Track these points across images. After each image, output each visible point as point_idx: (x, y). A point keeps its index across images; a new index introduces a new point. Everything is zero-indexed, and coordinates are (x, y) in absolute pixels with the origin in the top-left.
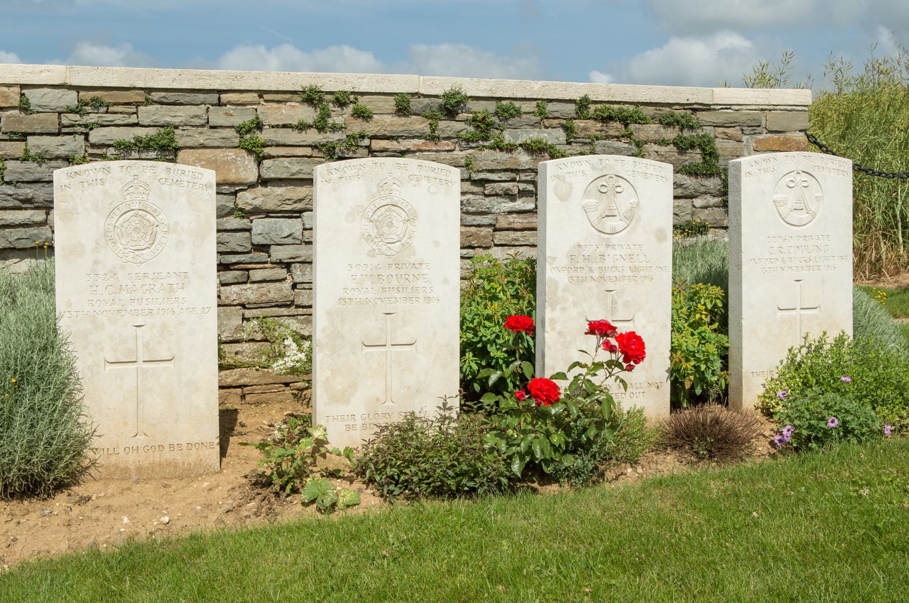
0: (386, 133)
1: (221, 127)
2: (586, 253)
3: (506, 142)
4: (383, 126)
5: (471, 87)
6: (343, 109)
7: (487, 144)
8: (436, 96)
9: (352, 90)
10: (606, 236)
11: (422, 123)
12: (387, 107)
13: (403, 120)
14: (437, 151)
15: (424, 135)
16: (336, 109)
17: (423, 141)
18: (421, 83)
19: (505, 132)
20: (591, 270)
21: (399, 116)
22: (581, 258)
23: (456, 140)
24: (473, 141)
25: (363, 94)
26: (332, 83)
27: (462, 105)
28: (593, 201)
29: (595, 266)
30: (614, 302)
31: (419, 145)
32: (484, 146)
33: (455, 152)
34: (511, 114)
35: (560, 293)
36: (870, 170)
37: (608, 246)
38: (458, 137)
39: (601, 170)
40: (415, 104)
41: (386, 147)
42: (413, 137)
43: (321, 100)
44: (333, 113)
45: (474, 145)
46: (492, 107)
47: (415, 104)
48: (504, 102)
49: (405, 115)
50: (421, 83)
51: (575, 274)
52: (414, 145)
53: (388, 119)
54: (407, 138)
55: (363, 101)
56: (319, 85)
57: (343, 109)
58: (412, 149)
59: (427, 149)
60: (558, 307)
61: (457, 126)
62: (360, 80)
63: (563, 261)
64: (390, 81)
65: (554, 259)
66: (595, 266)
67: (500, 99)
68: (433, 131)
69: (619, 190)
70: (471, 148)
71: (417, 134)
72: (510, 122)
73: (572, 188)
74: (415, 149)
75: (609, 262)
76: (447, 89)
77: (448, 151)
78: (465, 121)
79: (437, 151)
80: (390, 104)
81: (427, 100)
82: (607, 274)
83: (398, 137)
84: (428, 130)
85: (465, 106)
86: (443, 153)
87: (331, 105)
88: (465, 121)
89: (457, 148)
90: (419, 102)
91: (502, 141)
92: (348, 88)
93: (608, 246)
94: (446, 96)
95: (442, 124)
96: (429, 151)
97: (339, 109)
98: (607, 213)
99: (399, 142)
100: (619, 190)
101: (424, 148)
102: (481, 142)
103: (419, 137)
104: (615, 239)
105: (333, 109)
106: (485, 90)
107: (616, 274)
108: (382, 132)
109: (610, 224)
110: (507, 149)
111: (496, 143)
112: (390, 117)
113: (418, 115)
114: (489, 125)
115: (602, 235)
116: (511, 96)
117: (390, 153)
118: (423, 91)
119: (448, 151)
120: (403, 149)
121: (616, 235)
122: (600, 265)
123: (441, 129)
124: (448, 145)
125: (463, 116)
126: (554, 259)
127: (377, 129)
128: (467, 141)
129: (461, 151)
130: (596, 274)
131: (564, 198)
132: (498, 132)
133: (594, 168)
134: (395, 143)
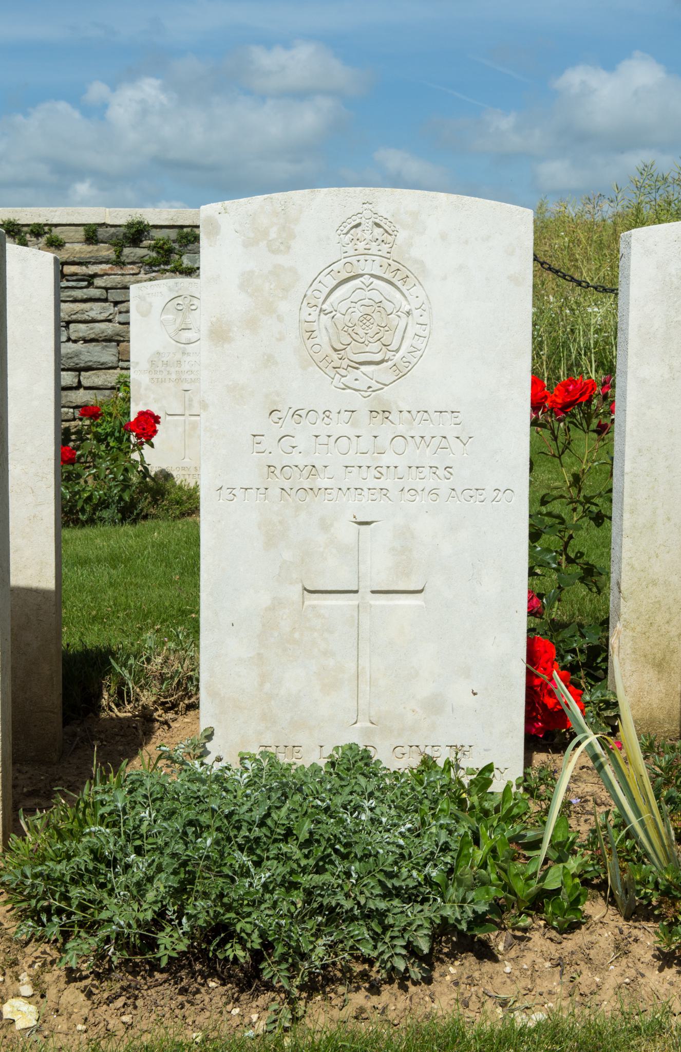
0: (75, 259)
1: (78, 242)
2: (165, 359)
3: (184, 266)
4: (72, 253)
5: (153, 215)
6: (38, 239)
7: (168, 267)
8: (120, 226)
9: (46, 222)
10: (183, 345)
11: (109, 250)
12: (77, 237)
13: (91, 247)
14: (123, 275)
15: (111, 261)
16: (33, 239)
17: (110, 266)
18: (107, 214)
19: (183, 257)
20: (169, 373)
21: (89, 244)
22: (160, 364)
23: (140, 265)
24: (155, 266)
25: (56, 225)
26: (28, 217)
27: (146, 233)
28: (170, 317)
29: (173, 370)
30: (191, 400)
31: (105, 270)
32: (165, 270)
33: (140, 276)
34: (189, 241)
35: (142, 391)
36: (600, 292)
37: (183, 353)
38: (141, 262)
39: (177, 292)
40: (102, 234)
41: (76, 271)
42: (101, 263)
43: (19, 232)
44: (29, 243)
45: (156, 269)
46: (173, 234)
47: (102, 234)
48: (185, 230)
49: (92, 243)
50: (107, 214)
51: (156, 376)
52: (102, 269)
53: (78, 247)
54: (94, 263)
55: (56, 231)
56: (17, 219)
57: (38, 239)
58: (100, 273)
59: (113, 272)
60: (141, 402)
61: (140, 252)
62: (53, 213)
63: (145, 365)
64: (79, 213)
65: (137, 363)
66: (173, 370)
67: (182, 227)
68: (118, 257)
69: (193, 307)
70: (154, 271)
71: (104, 260)
72: (189, 248)
73: (151, 306)
74: (102, 273)
75: (186, 367)
76: (130, 219)
77: (133, 274)
78: (149, 247)
79: (123, 275)
80: (81, 233)
81: (113, 230)
82: (183, 377)
83: (87, 262)
84: (113, 256)
85: (149, 234)
86: (128, 276)
87: (28, 236)
88: (149, 247)
89: (143, 272)
90: (106, 232)
91: (181, 265)
92: (42, 221)
93: (183, 353)
94: (130, 226)
95: (126, 251)
96: (115, 274)
97: (35, 239)
98: (183, 327)
99: (87, 267)
100: (193, 307)
101: (110, 272)
102: (162, 266)
103: (107, 262)
104: (189, 348)
105: (30, 239)
106: (166, 219)
107: (192, 376)
108: (72, 259)
109: (186, 335)
110: (186, 272)
111: (175, 267)
112: (80, 245)
113: (105, 243)
114: (170, 251)
115: (179, 344)
116: (191, 224)
117: (80, 277)
118: (109, 222)
119: (133, 274)
120: (91, 273)
121: (192, 345)
122: (177, 369)
123: (126, 255)
124: (133, 269)
125: (146, 243)
126: (137, 363)
127: (67, 256)
128: (151, 265)
129: (146, 274)
130: (174, 376)
131: (145, 314)
132: (177, 257)
133: (170, 290)
134: (84, 268)
